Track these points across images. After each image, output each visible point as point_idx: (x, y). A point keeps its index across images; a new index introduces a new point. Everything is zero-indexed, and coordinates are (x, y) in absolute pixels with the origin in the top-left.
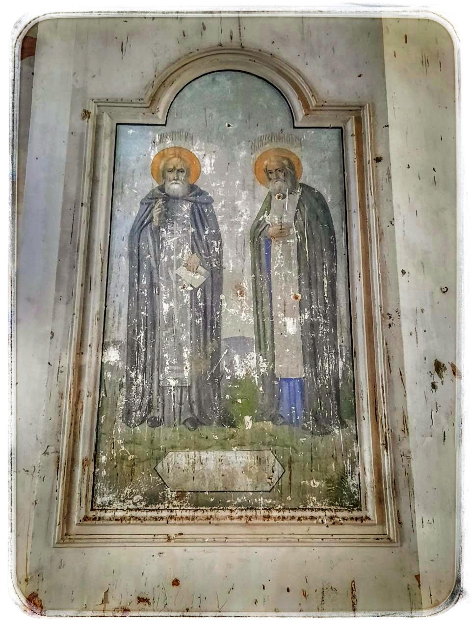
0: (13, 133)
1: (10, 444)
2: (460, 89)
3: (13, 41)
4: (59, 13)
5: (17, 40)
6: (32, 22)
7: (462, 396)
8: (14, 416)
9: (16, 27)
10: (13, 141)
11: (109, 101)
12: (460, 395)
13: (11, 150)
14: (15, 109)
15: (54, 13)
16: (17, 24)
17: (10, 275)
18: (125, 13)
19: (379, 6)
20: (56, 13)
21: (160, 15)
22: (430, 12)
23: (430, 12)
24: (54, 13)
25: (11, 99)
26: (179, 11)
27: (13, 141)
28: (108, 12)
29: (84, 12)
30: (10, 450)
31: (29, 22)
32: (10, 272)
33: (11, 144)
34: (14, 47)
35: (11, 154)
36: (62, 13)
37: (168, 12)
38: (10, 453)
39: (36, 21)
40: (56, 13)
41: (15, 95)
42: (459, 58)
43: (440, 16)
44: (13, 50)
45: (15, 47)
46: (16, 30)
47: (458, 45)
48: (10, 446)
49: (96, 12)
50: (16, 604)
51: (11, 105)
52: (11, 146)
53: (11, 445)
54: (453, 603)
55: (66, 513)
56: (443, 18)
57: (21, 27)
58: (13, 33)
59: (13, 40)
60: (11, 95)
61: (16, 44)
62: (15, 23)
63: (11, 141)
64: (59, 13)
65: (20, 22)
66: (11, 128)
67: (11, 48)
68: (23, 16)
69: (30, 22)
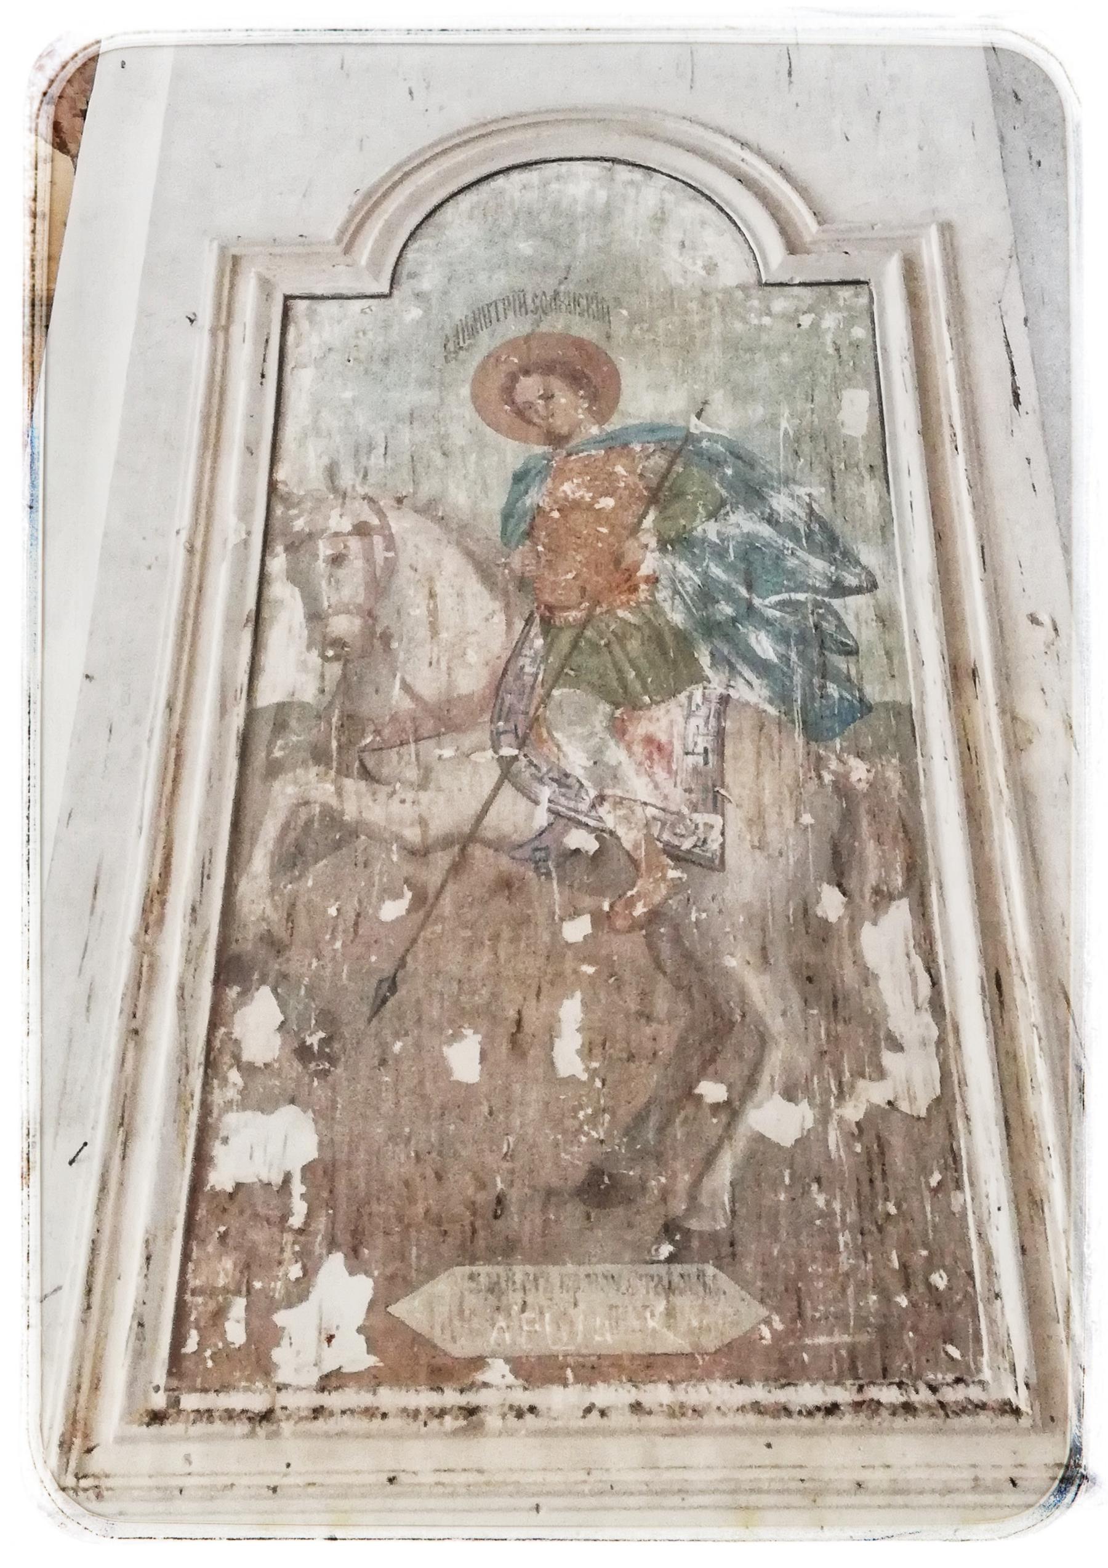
0: (33, 332)
1: (25, 1108)
2: (1079, 221)
3: (31, 104)
4: (148, 32)
5: (42, 101)
6: (80, 55)
7: (1085, 988)
8: (35, 1039)
9: (40, 68)
10: (32, 352)
11: (764, 1440)
12: (1081, 987)
13: (28, 374)
14: (38, 272)
15: (134, 33)
16: (43, 62)
17: (26, 688)
18: (312, 33)
19: (879, 16)
20: (140, 32)
21: (463, 36)
22: (1004, 30)
23: (1004, 30)
24: (134, 33)
25: (28, 248)
26: (300, 27)
27: (32, 352)
28: (269, 30)
29: (210, 31)
30: (25, 1122)
31: (71, 55)
32: (25, 678)
33: (28, 361)
34: (34, 116)
35: (28, 385)
36: (155, 32)
37: (658, 30)
38: (25, 1132)
39: (91, 52)
40: (140, 32)
41: (38, 238)
42: (1078, 146)
43: (1031, 40)
44: (34, 125)
45: (38, 116)
46: (39, 75)
47: (1072, 110)
48: (25, 1115)
49: (239, 30)
50: (40, 1507)
51: (28, 263)
52: (27, 365)
53: (28, 1111)
54: (1062, 1508)
55: (156, 907)
56: (1038, 45)
57: (52, 67)
58: (32, 84)
59: (32, 98)
60: (29, 238)
61: (39, 110)
62: (36, 57)
63: (28, 353)
64: (148, 32)
65: (50, 54)
66: (28, 319)
67: (27, 119)
68: (59, 40)
69: (76, 55)
